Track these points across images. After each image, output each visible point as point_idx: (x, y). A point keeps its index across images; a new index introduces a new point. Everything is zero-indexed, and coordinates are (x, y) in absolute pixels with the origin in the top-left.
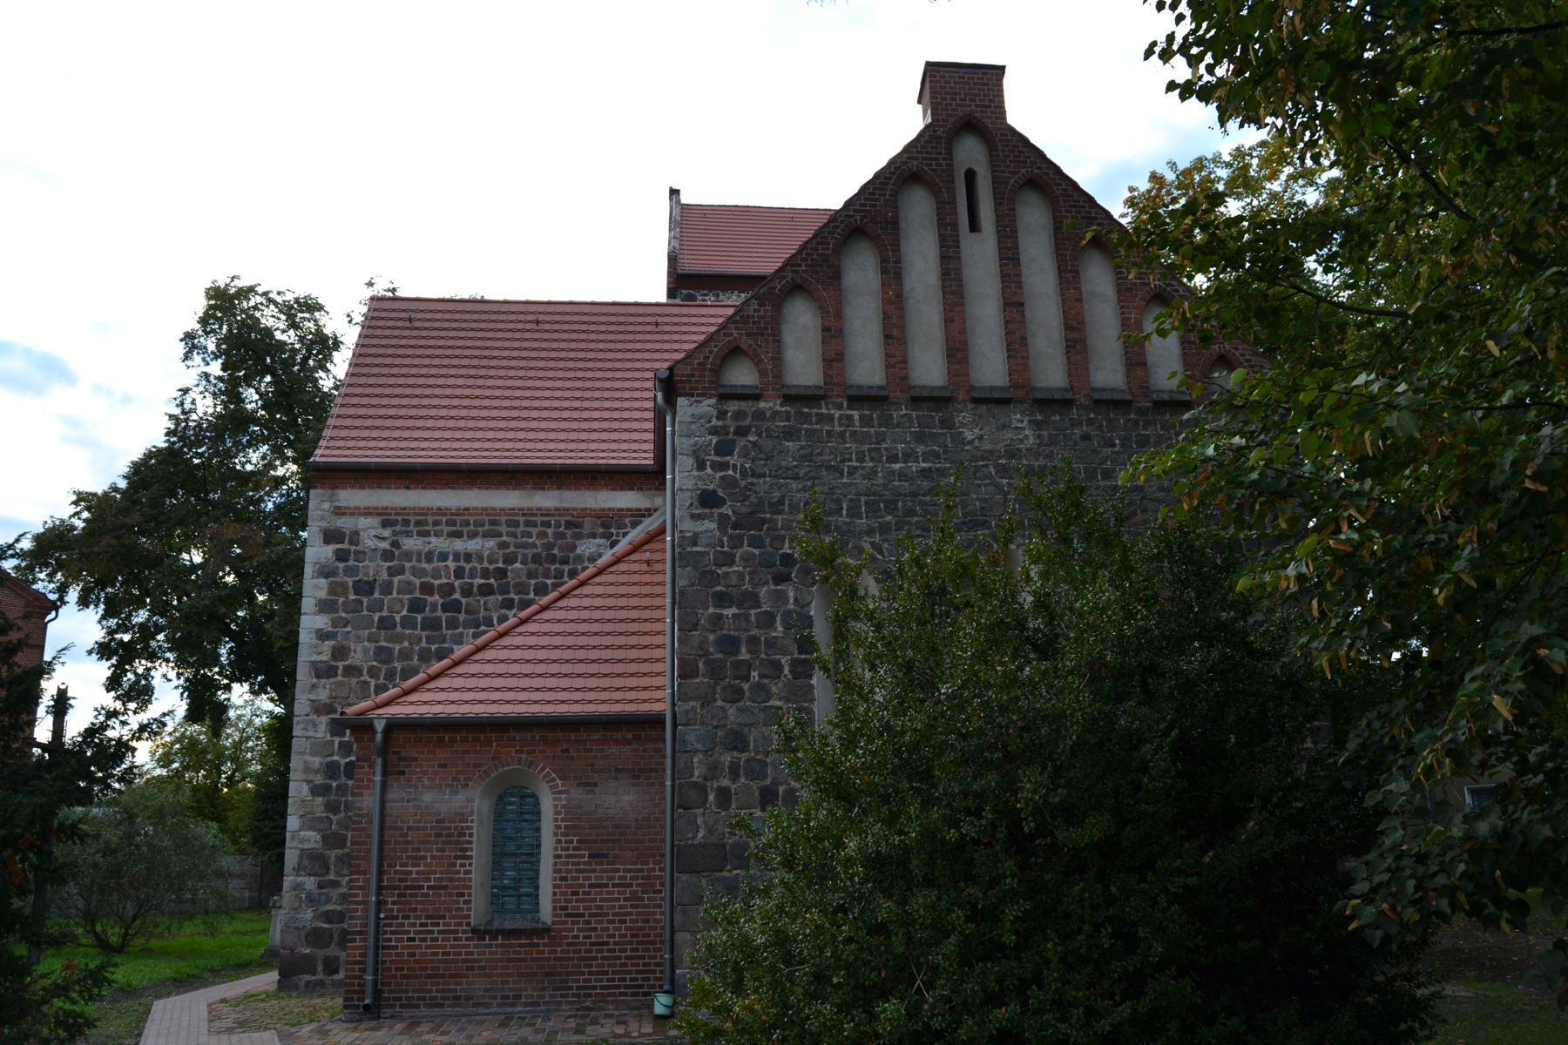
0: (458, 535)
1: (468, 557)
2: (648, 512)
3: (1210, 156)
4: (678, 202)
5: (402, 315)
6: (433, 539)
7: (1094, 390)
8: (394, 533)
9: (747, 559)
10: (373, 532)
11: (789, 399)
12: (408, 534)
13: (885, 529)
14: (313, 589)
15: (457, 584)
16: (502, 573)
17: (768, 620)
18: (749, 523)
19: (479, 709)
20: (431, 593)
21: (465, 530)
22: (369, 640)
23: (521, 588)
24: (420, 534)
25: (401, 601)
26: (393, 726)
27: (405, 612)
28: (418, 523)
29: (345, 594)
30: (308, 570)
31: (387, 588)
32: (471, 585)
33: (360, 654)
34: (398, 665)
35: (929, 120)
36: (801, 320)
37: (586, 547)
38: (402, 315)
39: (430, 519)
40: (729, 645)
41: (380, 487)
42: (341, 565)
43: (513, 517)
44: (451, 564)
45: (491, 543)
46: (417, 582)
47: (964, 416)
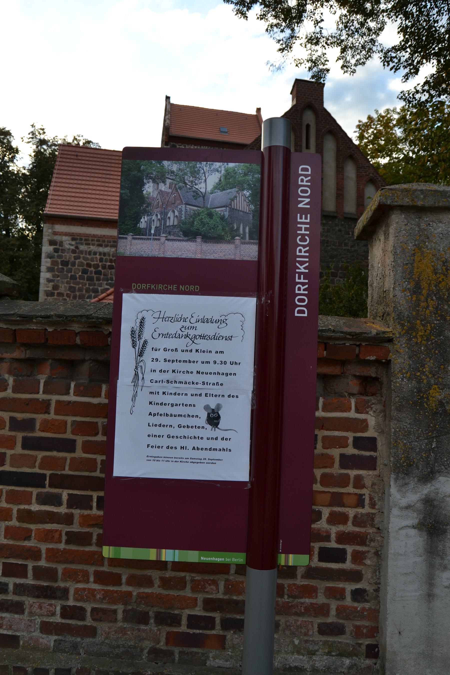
0: (100, 245)
1: (105, 254)
3: (392, 109)
4: (169, 102)
5: (73, 153)
6: (91, 246)
7: (345, 213)
8: (76, 243)
10: (68, 242)
12: (82, 244)
14: (45, 263)
15: (100, 264)
20: (90, 267)
21: (104, 244)
22: (67, 283)
24: (87, 244)
25: (79, 269)
27: (80, 274)
28: (86, 240)
29: (58, 266)
30: (43, 255)
31: (74, 264)
32: (106, 265)
33: (63, 288)
34: (78, 294)
35: (295, 103)
38: (73, 153)
39: (90, 239)
41: (71, 225)
42: (56, 254)
44: (98, 257)
46: (85, 262)
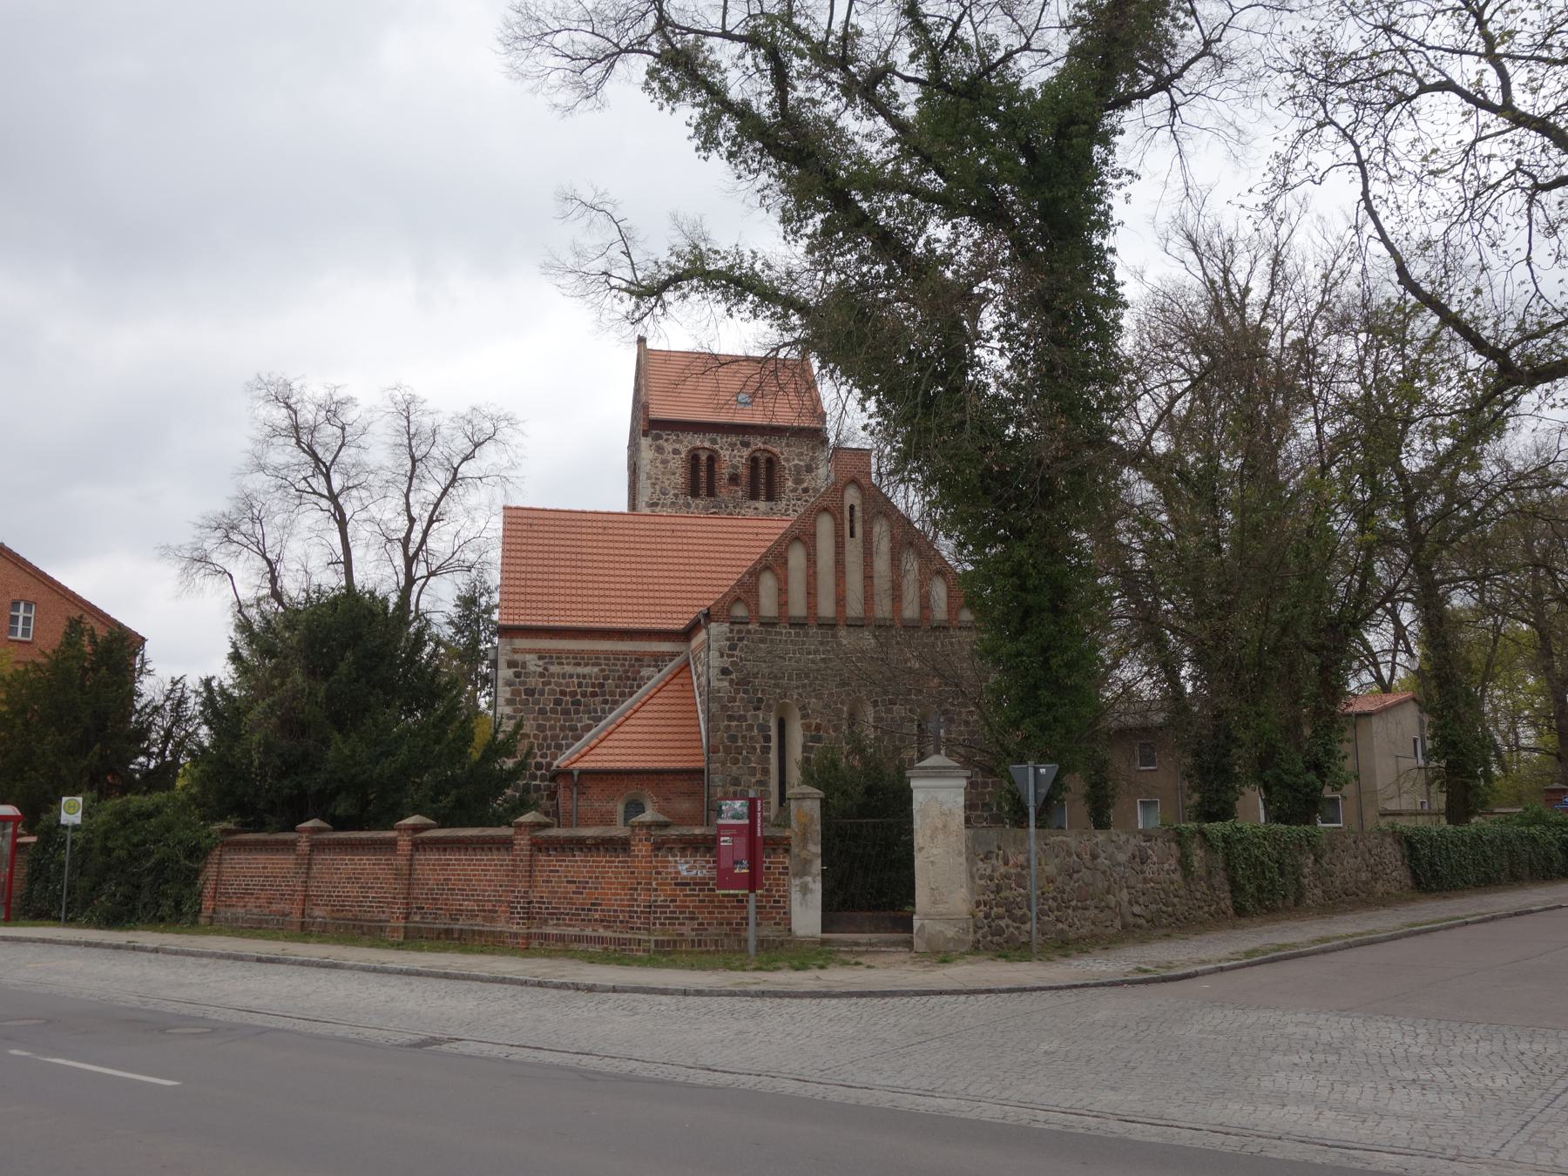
0: (579, 664)
1: (584, 677)
2: (678, 654)
9: (742, 699)
11: (762, 624)
13: (804, 686)
16: (602, 685)
17: (750, 728)
18: (743, 683)
19: (618, 765)
23: (612, 694)
26: (583, 772)
30: (500, 682)
31: (542, 693)
36: (768, 583)
37: (645, 672)
40: (733, 738)
43: (607, 655)
45: (596, 669)
47: (842, 633)
